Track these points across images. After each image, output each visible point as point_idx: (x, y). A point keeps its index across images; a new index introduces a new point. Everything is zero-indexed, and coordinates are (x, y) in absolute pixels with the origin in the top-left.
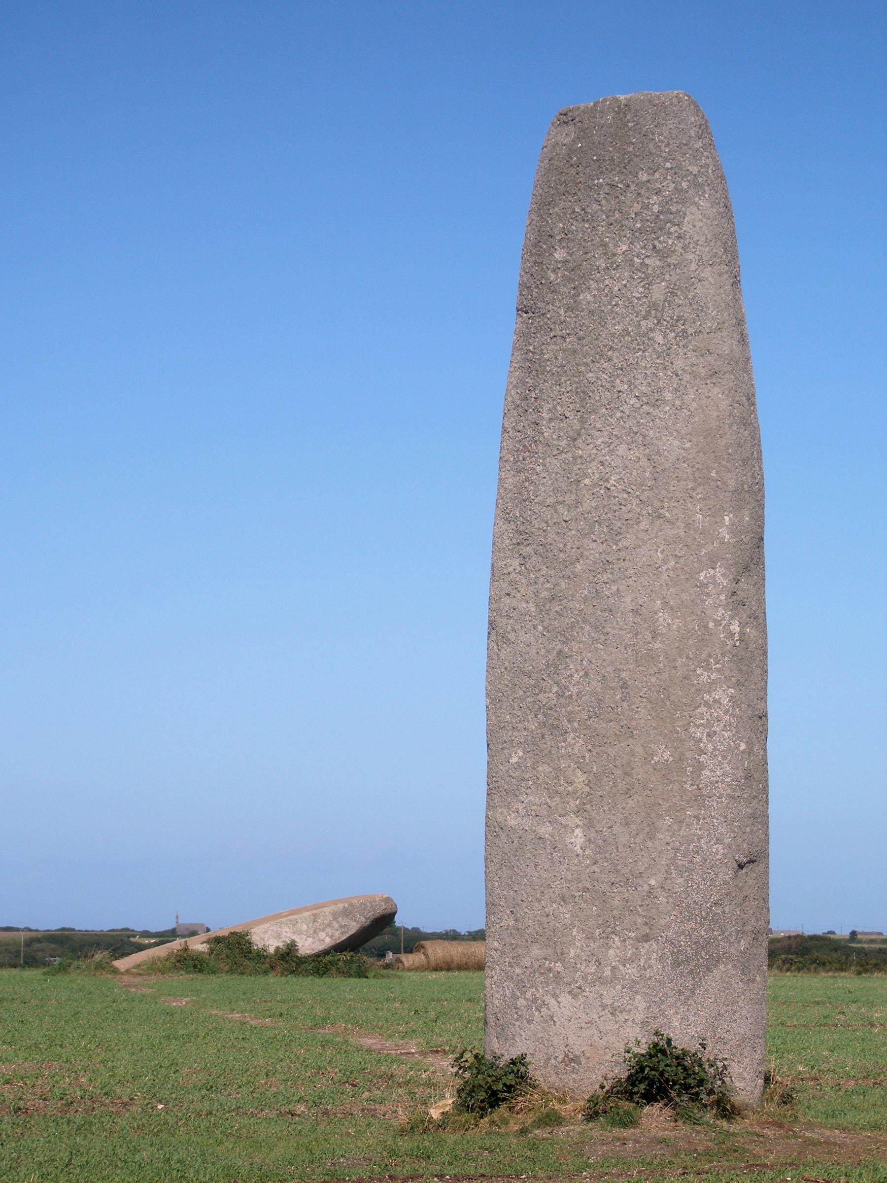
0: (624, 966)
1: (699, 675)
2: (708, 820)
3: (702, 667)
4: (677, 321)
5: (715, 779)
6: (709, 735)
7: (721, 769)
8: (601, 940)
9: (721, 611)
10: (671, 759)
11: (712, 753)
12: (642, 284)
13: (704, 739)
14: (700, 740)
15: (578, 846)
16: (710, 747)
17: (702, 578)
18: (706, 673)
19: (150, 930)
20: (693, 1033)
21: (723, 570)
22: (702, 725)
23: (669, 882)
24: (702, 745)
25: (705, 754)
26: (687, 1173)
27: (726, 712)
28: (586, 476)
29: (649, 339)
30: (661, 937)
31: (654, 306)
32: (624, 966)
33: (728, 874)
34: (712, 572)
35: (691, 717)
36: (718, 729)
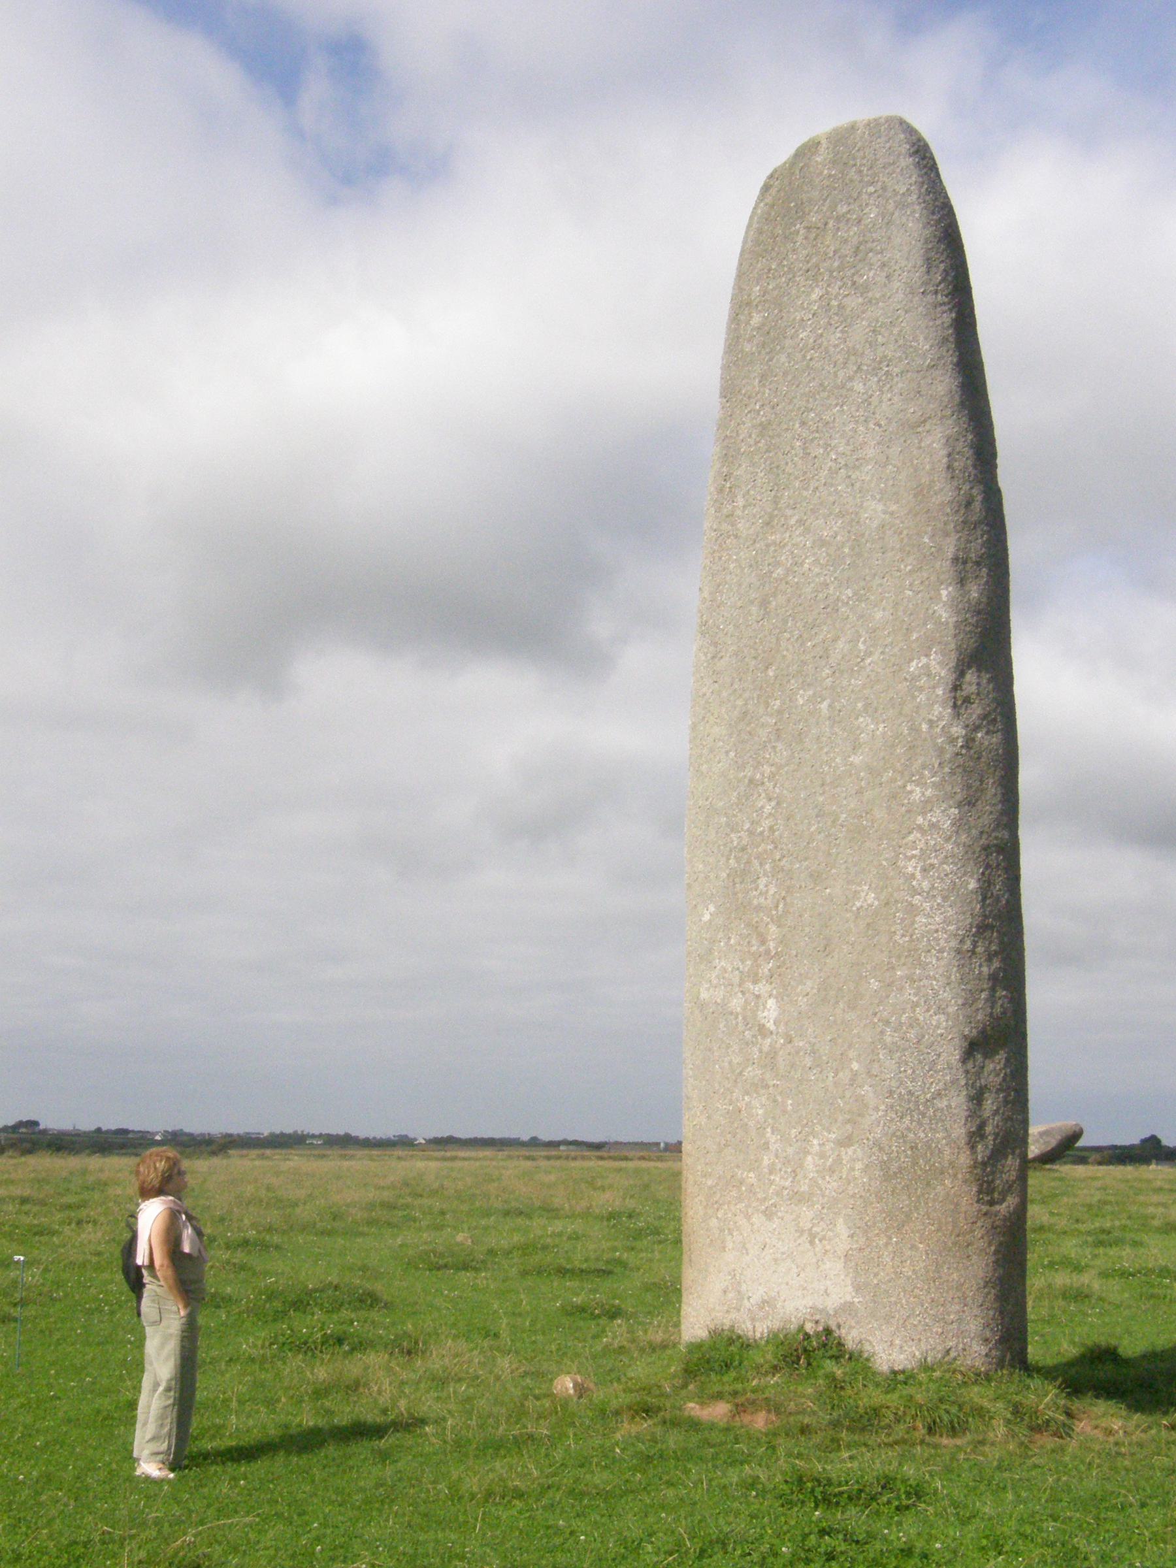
0: (824, 1178)
1: (911, 792)
2: (925, 982)
3: (913, 781)
4: (880, 362)
5: (933, 927)
6: (924, 870)
7: (941, 914)
8: (799, 1143)
9: (937, 709)
10: (876, 903)
11: (928, 893)
12: (840, 328)
13: (918, 875)
14: (913, 876)
15: (772, 1021)
16: (925, 885)
17: (912, 669)
18: (918, 789)
19: (494, 1137)
20: (910, 1273)
21: (939, 657)
22: (914, 856)
23: (876, 1065)
24: (914, 883)
25: (919, 894)
26: (331, 1550)
27: (948, 839)
28: (778, 564)
29: (848, 390)
30: (868, 1139)
31: (852, 352)
32: (824, 1178)
33: (953, 1055)
34: (924, 660)
35: (900, 847)
36: (936, 862)
